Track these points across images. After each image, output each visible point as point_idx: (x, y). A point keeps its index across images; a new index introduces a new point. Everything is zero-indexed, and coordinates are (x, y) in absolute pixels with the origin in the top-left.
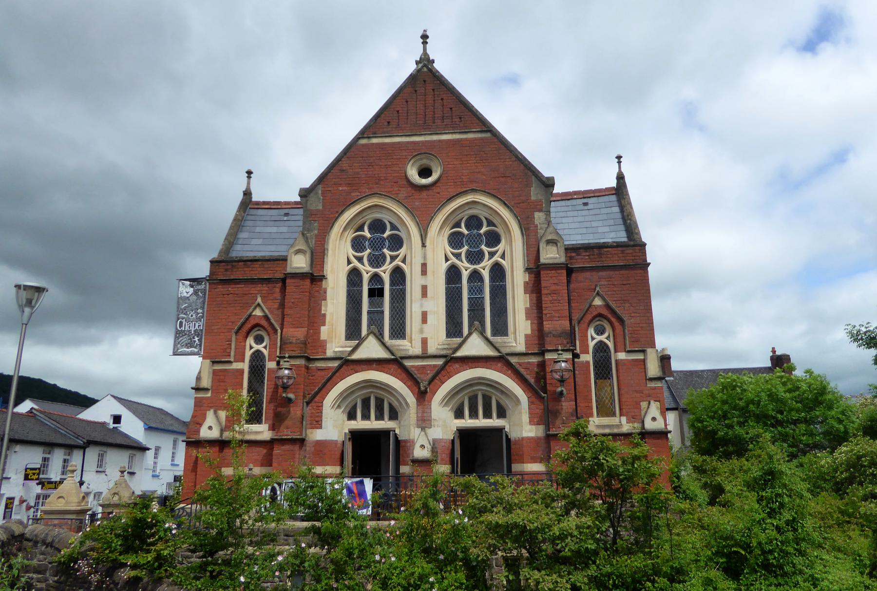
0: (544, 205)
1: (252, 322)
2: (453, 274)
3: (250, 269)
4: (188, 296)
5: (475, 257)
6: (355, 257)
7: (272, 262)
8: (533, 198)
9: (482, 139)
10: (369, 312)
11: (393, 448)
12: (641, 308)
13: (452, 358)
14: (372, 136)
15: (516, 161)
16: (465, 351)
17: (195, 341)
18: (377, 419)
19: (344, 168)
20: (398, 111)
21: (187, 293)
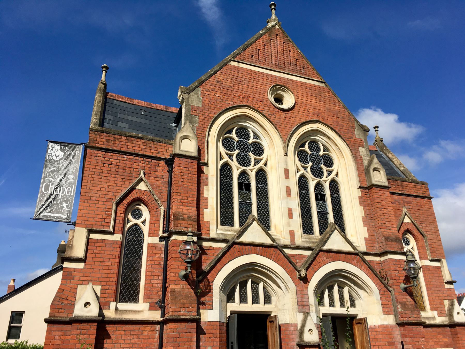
0: (364, 143)
1: (134, 195)
2: (60, 192)
3: (134, 145)
4: (58, 159)
7: (155, 143)
8: (357, 136)
9: (319, 87)
10: (240, 203)
11: (119, 283)
13: (321, 251)
14: (241, 61)
15: (343, 108)
16: (328, 246)
17: (63, 207)
19: (220, 80)
20: (259, 50)
21: (57, 156)
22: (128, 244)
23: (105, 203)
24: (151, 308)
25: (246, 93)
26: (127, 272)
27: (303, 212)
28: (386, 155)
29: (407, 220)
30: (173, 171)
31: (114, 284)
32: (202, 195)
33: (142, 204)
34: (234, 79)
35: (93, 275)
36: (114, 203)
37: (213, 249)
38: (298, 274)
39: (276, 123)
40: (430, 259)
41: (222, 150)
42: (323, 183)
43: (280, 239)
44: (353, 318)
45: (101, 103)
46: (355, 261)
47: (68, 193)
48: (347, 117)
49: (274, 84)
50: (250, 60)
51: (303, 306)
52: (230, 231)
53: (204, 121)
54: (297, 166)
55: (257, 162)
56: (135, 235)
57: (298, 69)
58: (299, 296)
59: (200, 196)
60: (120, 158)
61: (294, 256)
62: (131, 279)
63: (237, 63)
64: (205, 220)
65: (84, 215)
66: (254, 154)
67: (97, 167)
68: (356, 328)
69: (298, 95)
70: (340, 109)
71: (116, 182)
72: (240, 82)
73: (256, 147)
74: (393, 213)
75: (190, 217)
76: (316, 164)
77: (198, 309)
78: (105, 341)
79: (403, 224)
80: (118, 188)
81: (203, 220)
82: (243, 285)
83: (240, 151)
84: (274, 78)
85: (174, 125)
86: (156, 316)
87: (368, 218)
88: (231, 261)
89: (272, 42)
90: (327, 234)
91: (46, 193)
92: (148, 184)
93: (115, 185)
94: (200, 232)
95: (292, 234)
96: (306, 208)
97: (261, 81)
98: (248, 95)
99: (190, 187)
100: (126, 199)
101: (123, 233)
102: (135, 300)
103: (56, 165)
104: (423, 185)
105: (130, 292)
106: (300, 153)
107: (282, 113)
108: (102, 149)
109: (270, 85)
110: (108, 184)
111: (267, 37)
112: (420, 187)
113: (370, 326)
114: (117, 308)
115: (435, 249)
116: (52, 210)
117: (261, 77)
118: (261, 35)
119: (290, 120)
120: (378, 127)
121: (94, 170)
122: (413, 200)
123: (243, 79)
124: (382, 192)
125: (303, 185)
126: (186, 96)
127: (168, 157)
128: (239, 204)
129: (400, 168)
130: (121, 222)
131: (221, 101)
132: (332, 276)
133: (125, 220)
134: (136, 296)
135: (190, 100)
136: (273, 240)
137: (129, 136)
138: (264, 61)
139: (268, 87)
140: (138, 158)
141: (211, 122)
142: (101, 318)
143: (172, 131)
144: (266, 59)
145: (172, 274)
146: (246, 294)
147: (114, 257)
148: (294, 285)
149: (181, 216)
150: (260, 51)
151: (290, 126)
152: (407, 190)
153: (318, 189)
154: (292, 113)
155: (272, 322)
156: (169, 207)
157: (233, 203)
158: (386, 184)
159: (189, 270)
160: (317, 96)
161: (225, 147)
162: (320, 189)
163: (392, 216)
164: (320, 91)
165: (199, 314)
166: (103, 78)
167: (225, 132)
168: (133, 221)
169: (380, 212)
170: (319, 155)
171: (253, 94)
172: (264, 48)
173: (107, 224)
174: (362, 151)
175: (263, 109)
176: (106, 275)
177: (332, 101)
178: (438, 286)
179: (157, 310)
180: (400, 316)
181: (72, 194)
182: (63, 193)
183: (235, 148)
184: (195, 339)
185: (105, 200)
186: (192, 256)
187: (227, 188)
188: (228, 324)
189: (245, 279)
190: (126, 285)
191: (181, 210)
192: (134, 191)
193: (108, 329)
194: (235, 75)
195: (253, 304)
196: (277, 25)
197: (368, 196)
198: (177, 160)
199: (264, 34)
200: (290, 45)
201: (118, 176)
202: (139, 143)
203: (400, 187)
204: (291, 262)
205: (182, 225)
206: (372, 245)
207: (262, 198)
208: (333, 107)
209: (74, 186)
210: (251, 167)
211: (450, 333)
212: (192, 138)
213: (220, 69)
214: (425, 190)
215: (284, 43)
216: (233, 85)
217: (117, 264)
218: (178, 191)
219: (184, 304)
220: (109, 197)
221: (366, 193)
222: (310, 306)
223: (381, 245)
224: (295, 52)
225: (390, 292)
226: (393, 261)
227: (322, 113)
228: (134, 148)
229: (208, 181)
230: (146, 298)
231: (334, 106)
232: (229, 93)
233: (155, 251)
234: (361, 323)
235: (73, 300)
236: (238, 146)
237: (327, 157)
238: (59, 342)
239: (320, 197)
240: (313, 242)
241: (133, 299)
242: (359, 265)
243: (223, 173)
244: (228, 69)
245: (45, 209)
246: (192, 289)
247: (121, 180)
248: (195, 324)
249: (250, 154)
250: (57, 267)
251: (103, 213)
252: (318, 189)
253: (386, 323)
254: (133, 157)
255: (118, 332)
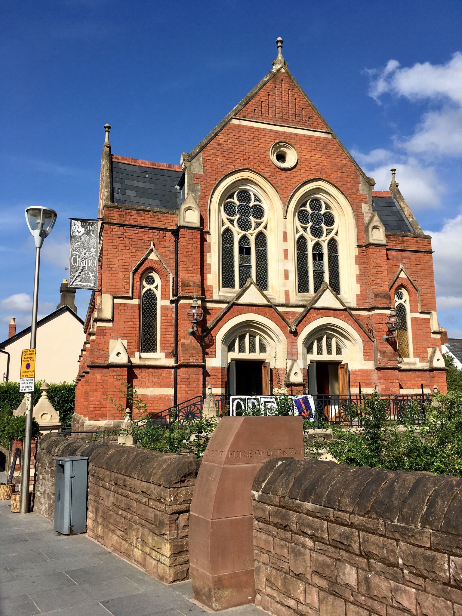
1: (146, 265)
2: (301, 243)
3: (143, 218)
4: (80, 235)
5: (317, 232)
6: (302, 227)
7: (162, 215)
8: (361, 192)
10: (240, 266)
12: (428, 283)
14: (243, 118)
15: (349, 161)
17: (90, 277)
18: (251, 351)
19: (221, 142)
20: (262, 102)
21: (79, 232)
22: (145, 306)
23: (124, 273)
24: (167, 356)
25: (247, 154)
26: (146, 329)
27: (300, 272)
28: (398, 203)
29: (402, 275)
30: (179, 241)
31: (137, 338)
32: (205, 262)
33: (154, 272)
34: (235, 139)
35: (120, 332)
36: (131, 272)
37: (216, 309)
38: (289, 328)
39: (277, 185)
40: (420, 311)
41: (224, 215)
42: (322, 243)
43: (275, 299)
44: (337, 364)
45: (108, 172)
46: (343, 316)
47: (93, 265)
48: (352, 171)
49: (277, 141)
50: (253, 115)
51: (293, 354)
52: (230, 293)
53: (206, 189)
54: (296, 227)
55: (257, 225)
56: (150, 298)
57: (303, 119)
58: (289, 347)
59: (203, 263)
60: (132, 232)
61: (287, 313)
62: (149, 334)
63: (238, 120)
64: (208, 284)
65: (108, 284)
66: (255, 218)
67: (114, 241)
68: (340, 371)
69: (301, 152)
70: (345, 162)
71: (131, 254)
72: (241, 143)
73: (256, 210)
74: (386, 271)
75: (195, 283)
76: (316, 223)
77: (204, 358)
78: (134, 380)
79: (398, 279)
80: (133, 259)
81: (206, 285)
82: (242, 338)
83: (242, 215)
84: (277, 134)
85: (178, 187)
86: (171, 362)
87: (362, 275)
88: (230, 319)
89: (276, 91)
90: (319, 293)
91: (75, 266)
92: (158, 254)
93: (130, 256)
94: (204, 297)
95: (287, 293)
96: (303, 268)
97: (263, 139)
98: (249, 156)
99: (194, 256)
100: (140, 269)
101: (140, 298)
102: (153, 350)
103: (79, 240)
104: (426, 240)
105: (149, 344)
106: (301, 213)
107: (283, 173)
108: (117, 224)
109: (272, 143)
110: (124, 256)
111: (271, 85)
112: (422, 242)
113: (352, 371)
114: (140, 357)
115: (427, 302)
116: (81, 280)
117: (263, 134)
118: (265, 84)
119: (292, 179)
120: (395, 170)
121: (111, 244)
122: (413, 256)
123: (244, 139)
124: (378, 250)
125: (302, 245)
126: (188, 164)
127: (175, 228)
128: (240, 267)
129: (409, 219)
130: (138, 288)
131: (222, 165)
132: (321, 330)
133: (141, 287)
134: (154, 347)
135: (192, 167)
136: (268, 300)
137: (138, 210)
138: (267, 115)
139: (270, 145)
140: (147, 230)
141: (213, 190)
142: (130, 364)
143: (177, 195)
144: (270, 111)
145: (182, 331)
146: (245, 345)
147: (135, 318)
148: (285, 338)
149: (188, 283)
150: (263, 103)
151: (291, 187)
152: (408, 245)
153: (316, 248)
154: (293, 173)
155: (265, 367)
156: (177, 274)
157: (234, 267)
158: (384, 242)
159: (195, 329)
160: (322, 149)
161: (226, 212)
162: (319, 248)
163: (385, 273)
164: (326, 143)
165: (204, 361)
166: (106, 140)
167: (226, 197)
168: (148, 287)
169: (374, 270)
170: (320, 214)
171: (254, 155)
172: (267, 98)
173: (127, 291)
174: (365, 208)
175: (264, 171)
176: (130, 332)
177: (338, 154)
178: (424, 336)
179: (171, 358)
180: (378, 362)
181: (96, 266)
182: (88, 264)
183: (237, 213)
184: (202, 379)
185: (123, 270)
186: (197, 318)
187: (228, 253)
188: (228, 369)
189: (244, 333)
190: (146, 339)
191: (187, 278)
192: (147, 261)
193: (135, 371)
194: (237, 135)
195: (250, 353)
196: (282, 69)
197: (365, 254)
198: (182, 231)
199: (268, 81)
200: (297, 91)
201: (132, 248)
202: (148, 216)
203: (400, 242)
204: (283, 319)
205: (189, 291)
206: (363, 301)
207: (261, 260)
208: (338, 161)
209: (96, 258)
210: (251, 231)
211: (428, 376)
212: (195, 209)
213: (221, 130)
214: (427, 244)
215: (289, 90)
216: (233, 147)
217: (137, 323)
218: (185, 260)
219: (192, 354)
220: (126, 267)
221: (363, 252)
222: (298, 355)
223: (371, 300)
224: (302, 100)
225: (373, 342)
226: (379, 316)
227: (326, 170)
228: (143, 221)
229: (210, 248)
230: (163, 349)
231: (340, 159)
232: (230, 156)
233: (167, 312)
234: (343, 368)
235: (107, 350)
236: (239, 210)
237: (328, 216)
238: (100, 381)
239: (318, 256)
240: (306, 301)
241: (152, 350)
242: (346, 320)
243: (225, 238)
244: (229, 128)
245: (76, 279)
246: (199, 342)
247: (134, 251)
248: (202, 368)
249: (251, 218)
250: (62, 307)
251: (123, 281)
252: (316, 248)
253: (365, 368)
254: (143, 230)
255: (143, 374)
